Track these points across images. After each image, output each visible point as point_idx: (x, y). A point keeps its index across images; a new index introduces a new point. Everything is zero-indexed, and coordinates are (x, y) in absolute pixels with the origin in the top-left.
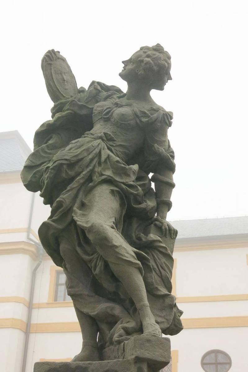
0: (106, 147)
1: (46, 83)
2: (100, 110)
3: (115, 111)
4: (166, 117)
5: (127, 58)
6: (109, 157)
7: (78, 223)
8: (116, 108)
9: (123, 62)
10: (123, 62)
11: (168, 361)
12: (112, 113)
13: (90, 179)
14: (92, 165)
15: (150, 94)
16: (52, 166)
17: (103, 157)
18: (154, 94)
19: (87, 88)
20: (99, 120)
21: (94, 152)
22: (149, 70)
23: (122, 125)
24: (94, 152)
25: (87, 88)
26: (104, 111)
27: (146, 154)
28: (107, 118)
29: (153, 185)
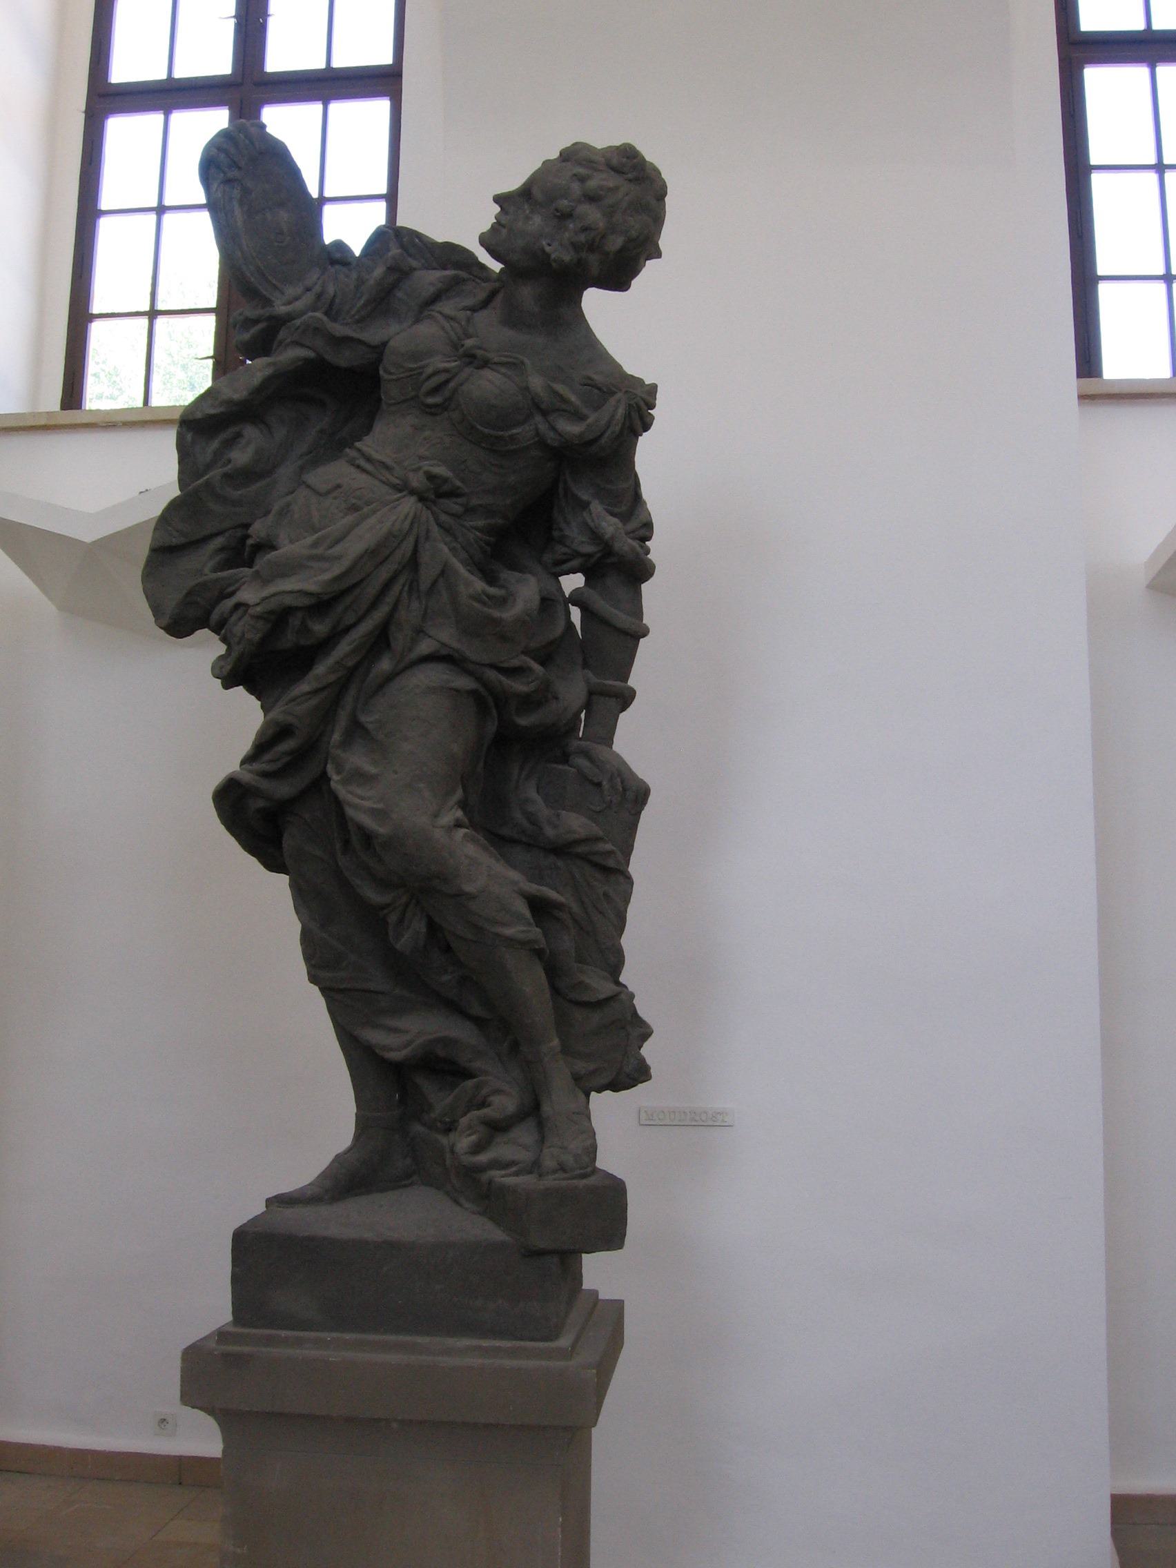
0: (435, 530)
1: (216, 237)
2: (411, 370)
3: (464, 388)
4: (635, 415)
5: (513, 182)
6: (445, 572)
7: (350, 812)
8: (468, 370)
9: (498, 199)
10: (498, 199)
11: (246, 766)
12: (455, 391)
13: (380, 640)
14: (390, 599)
15: (583, 305)
16: (258, 609)
17: (427, 574)
18: (597, 305)
19: (357, 248)
20: (404, 401)
21: (398, 556)
22: (592, 221)
23: (487, 432)
24: (398, 556)
25: (357, 248)
26: (429, 377)
27: (557, 488)
28: (437, 400)
29: (576, 614)
